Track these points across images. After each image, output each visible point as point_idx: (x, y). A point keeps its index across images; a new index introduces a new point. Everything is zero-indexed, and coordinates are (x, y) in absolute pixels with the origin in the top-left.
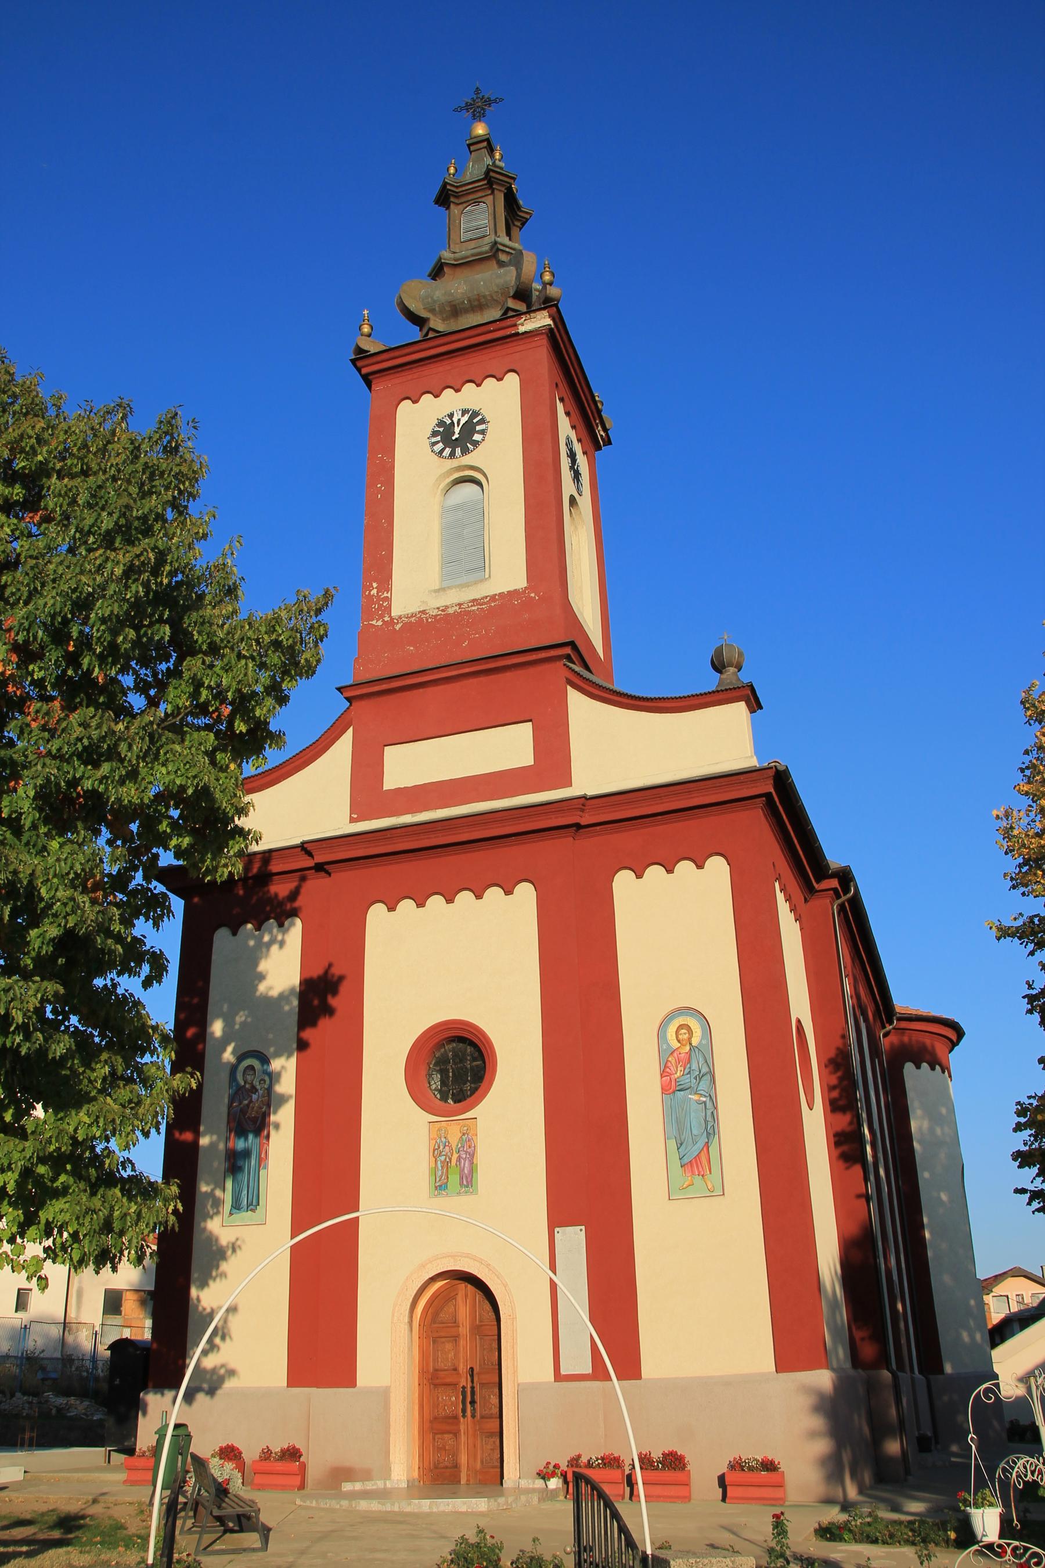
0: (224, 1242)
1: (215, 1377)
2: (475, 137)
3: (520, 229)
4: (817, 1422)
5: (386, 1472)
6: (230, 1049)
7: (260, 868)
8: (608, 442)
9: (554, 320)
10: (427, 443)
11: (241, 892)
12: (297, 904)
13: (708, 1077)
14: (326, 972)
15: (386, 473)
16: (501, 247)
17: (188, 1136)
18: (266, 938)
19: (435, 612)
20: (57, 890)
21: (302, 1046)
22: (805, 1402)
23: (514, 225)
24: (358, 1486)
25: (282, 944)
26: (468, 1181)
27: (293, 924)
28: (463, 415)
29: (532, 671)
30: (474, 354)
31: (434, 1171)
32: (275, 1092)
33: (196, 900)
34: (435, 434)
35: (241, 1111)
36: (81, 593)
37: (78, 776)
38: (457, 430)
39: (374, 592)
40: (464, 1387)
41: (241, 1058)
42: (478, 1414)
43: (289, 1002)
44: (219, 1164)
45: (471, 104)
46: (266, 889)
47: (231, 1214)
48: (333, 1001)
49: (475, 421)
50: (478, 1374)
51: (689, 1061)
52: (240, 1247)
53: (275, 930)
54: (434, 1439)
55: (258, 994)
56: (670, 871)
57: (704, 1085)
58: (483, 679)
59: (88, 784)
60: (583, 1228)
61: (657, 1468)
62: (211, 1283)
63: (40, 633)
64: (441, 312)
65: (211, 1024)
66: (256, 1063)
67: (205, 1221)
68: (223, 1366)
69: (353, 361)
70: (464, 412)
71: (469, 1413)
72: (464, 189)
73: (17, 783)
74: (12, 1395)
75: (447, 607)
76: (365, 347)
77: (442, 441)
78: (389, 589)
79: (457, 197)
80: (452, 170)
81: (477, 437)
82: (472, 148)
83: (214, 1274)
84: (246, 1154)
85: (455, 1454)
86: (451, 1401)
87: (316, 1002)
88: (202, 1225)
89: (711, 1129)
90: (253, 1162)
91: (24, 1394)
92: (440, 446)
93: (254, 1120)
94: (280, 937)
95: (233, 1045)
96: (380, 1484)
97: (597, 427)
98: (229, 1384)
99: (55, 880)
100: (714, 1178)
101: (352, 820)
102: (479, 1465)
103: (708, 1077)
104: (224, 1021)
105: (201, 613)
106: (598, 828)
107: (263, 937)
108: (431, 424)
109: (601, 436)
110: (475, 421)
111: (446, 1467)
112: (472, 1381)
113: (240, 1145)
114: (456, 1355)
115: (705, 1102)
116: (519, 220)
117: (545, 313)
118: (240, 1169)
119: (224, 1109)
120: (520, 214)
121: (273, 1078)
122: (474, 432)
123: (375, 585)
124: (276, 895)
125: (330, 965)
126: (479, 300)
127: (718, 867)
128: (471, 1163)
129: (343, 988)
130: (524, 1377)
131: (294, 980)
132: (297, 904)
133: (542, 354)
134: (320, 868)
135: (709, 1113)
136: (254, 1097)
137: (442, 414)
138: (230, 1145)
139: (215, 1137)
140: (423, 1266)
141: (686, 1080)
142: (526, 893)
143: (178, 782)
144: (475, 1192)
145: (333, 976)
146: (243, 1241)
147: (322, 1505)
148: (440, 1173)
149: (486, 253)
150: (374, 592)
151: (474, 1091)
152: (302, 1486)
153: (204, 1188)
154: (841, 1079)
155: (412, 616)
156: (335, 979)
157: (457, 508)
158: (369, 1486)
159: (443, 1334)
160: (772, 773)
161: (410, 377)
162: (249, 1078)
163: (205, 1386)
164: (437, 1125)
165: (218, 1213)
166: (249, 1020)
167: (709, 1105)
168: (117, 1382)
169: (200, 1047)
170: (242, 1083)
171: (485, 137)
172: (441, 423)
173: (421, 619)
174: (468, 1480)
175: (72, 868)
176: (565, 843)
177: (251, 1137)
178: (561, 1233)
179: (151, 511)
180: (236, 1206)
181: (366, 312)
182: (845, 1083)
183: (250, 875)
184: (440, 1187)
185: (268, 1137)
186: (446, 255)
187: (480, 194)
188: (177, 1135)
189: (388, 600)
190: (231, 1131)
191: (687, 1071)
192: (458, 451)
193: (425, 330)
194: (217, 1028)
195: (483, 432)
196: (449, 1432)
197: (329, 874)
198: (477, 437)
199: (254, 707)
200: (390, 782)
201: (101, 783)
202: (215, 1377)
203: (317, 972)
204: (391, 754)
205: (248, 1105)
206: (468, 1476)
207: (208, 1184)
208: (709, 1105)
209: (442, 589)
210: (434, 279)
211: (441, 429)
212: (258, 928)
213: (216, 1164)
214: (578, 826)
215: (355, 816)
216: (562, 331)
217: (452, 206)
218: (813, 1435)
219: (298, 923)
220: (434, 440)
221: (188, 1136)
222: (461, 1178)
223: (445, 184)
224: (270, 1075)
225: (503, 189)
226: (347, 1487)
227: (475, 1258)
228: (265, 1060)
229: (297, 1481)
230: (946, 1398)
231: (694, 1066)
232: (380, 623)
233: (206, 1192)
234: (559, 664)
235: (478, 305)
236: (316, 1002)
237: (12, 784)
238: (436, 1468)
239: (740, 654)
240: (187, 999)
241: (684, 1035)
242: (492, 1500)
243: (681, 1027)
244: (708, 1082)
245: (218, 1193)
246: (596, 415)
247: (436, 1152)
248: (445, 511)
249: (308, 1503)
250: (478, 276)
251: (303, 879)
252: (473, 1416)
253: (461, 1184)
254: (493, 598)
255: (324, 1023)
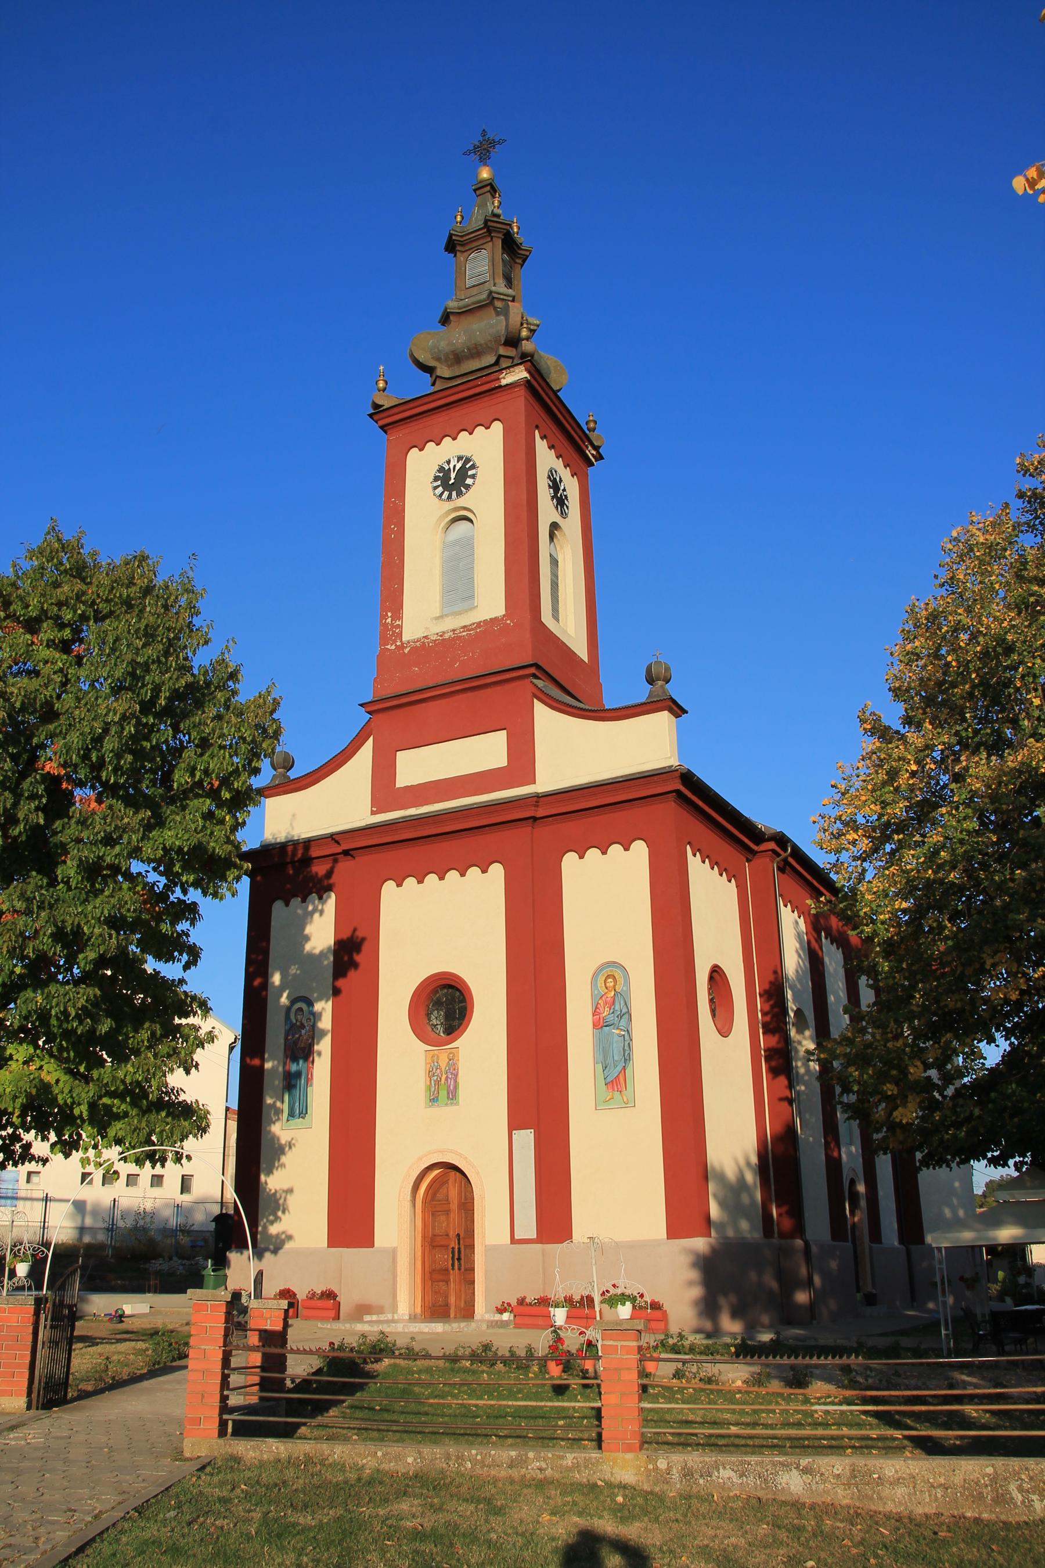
0: (283, 1141)
1: (278, 1241)
2: (481, 182)
3: (522, 266)
4: (694, 1275)
5: (394, 1309)
6: (285, 995)
7: (303, 854)
8: (600, 457)
9: (529, 372)
10: (430, 487)
11: (291, 872)
12: (331, 881)
13: (627, 1016)
14: (352, 936)
15: (395, 515)
16: (496, 296)
17: (256, 1062)
18: (310, 908)
19: (434, 638)
20: (94, 927)
21: (336, 992)
22: (686, 1260)
23: (516, 263)
24: (374, 1318)
25: (322, 912)
26: (453, 1095)
27: (329, 897)
28: (458, 462)
29: (507, 687)
30: (465, 406)
31: (429, 1088)
32: (318, 1028)
33: (259, 878)
34: (436, 479)
35: (294, 1042)
36: (94, 734)
37: (101, 854)
38: (453, 475)
39: (389, 620)
40: (453, 1248)
41: (293, 1002)
42: (463, 1268)
43: (327, 958)
44: (278, 1083)
45: (478, 147)
46: (309, 869)
47: (288, 1120)
48: (357, 958)
49: (467, 466)
50: (463, 1238)
51: (614, 1003)
52: (294, 1145)
53: (316, 902)
54: (432, 1285)
55: (305, 951)
56: (604, 853)
57: (623, 1022)
58: (470, 694)
59: (108, 859)
60: (532, 1130)
61: (575, 1307)
62: (275, 1171)
63: (74, 756)
64: (446, 360)
65: (272, 976)
66: (304, 1006)
67: (270, 1125)
68: (283, 1232)
69: (371, 416)
70: (460, 458)
71: (456, 1267)
72: (467, 237)
73: (66, 857)
74: (170, 1259)
75: (444, 633)
76: (380, 403)
77: (442, 485)
78: (401, 618)
79: (462, 245)
80: (459, 219)
81: (469, 481)
82: (478, 192)
83: (276, 1165)
84: (298, 1074)
85: (446, 1297)
86: (444, 1258)
87: (346, 958)
88: (268, 1128)
89: (627, 1058)
90: (303, 1082)
91: (180, 1258)
92: (440, 489)
93: (303, 1049)
94: (320, 907)
95: (287, 992)
96: (390, 1316)
97: (587, 448)
98: (288, 1246)
99: (93, 921)
100: (627, 1094)
101: (373, 813)
102: (462, 1304)
103: (627, 1016)
104: (281, 974)
105: (192, 719)
106: (551, 819)
107: (308, 907)
108: (433, 471)
109: (592, 455)
110: (467, 466)
111: (440, 1306)
112: (459, 1243)
113: (294, 1068)
114: (448, 1224)
115: (624, 1035)
116: (520, 258)
117: (522, 367)
118: (295, 1086)
119: (282, 1041)
120: (520, 252)
121: (316, 1017)
122: (467, 476)
123: (389, 614)
124: (317, 874)
125: (355, 930)
126: (476, 348)
127: (640, 849)
128: (456, 1081)
129: (365, 948)
130: (491, 1240)
131: (331, 942)
132: (331, 881)
133: (520, 402)
134: (346, 853)
135: (626, 1044)
136: (303, 1032)
137: (441, 461)
138: (287, 1068)
139: (276, 1062)
140: (420, 1159)
141: (611, 1018)
142: (497, 870)
143: (177, 843)
144: (457, 1104)
145: (357, 938)
146: (297, 1140)
147: (334, 1327)
148: (433, 1089)
149: (485, 300)
150: (389, 620)
151: (460, 1025)
152: (337, 1317)
153: (269, 1101)
154: (772, 1007)
155: (418, 641)
156: (359, 940)
157: (455, 543)
158: (382, 1317)
159: (438, 1209)
160: (677, 774)
161: (531, 401)
162: (299, 1017)
163: (272, 1247)
164: (432, 1053)
165: (278, 1119)
166: (298, 972)
167: (627, 1037)
168: (221, 1245)
169: (264, 993)
170: (940, 1099)
171: (490, 181)
172: (441, 469)
173: (424, 643)
174: (455, 1315)
175: (102, 913)
176: (525, 831)
177: (301, 1062)
178: (516, 1134)
179: (149, 657)
180: (291, 1115)
181: (381, 368)
182: (776, 1010)
183: (296, 859)
184: (433, 1100)
185: (313, 1062)
186: (452, 305)
187: (481, 242)
188: (248, 1060)
189: (400, 627)
190: (287, 1058)
191: (612, 1011)
192: (454, 493)
193: (434, 377)
194: (276, 979)
195: (473, 477)
196: (442, 1281)
197: (354, 857)
198: (469, 481)
199: (233, 781)
200: (401, 781)
201: (116, 858)
202: (278, 1241)
203: (346, 935)
204: (403, 758)
205: (299, 1038)
206: (456, 1312)
207: (272, 1098)
208: (627, 1037)
209: (441, 617)
210: (443, 325)
211: (441, 475)
212: (304, 901)
213: (277, 1082)
214: (535, 819)
215: (375, 809)
216: (539, 379)
217: (458, 254)
218: (691, 1283)
219: (333, 895)
220: (436, 484)
221: (256, 1062)
222: (448, 1093)
223: (451, 235)
224: (314, 1014)
225: (500, 235)
226: (367, 1318)
227: (456, 1153)
228: (310, 1004)
229: (332, 1313)
230: (925, 1264)
231: (617, 1007)
232: (393, 647)
233: (270, 1104)
234: (527, 681)
235: (476, 352)
236: (346, 958)
237: (63, 858)
238: (434, 1306)
239: (668, 669)
240: (253, 956)
241: (610, 983)
242: (447, 1325)
243: (608, 977)
244: (626, 1020)
245: (279, 1104)
246: (584, 439)
247: (430, 1074)
248: (446, 546)
249: (325, 1326)
250: (475, 326)
251: (336, 861)
252: (459, 1269)
253: (448, 1097)
254: (479, 624)
255: (352, 974)
